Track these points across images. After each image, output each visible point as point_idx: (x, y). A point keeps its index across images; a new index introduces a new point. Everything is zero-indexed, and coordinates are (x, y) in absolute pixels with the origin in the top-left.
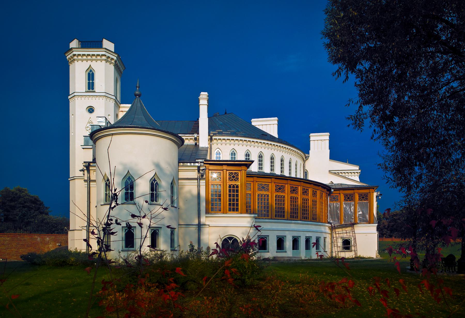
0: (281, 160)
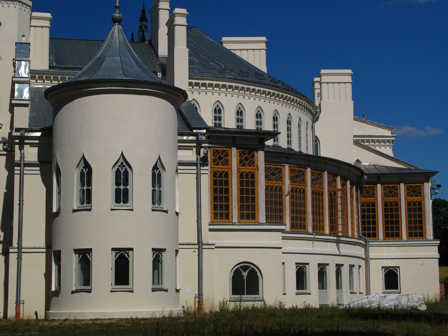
0: (274, 118)
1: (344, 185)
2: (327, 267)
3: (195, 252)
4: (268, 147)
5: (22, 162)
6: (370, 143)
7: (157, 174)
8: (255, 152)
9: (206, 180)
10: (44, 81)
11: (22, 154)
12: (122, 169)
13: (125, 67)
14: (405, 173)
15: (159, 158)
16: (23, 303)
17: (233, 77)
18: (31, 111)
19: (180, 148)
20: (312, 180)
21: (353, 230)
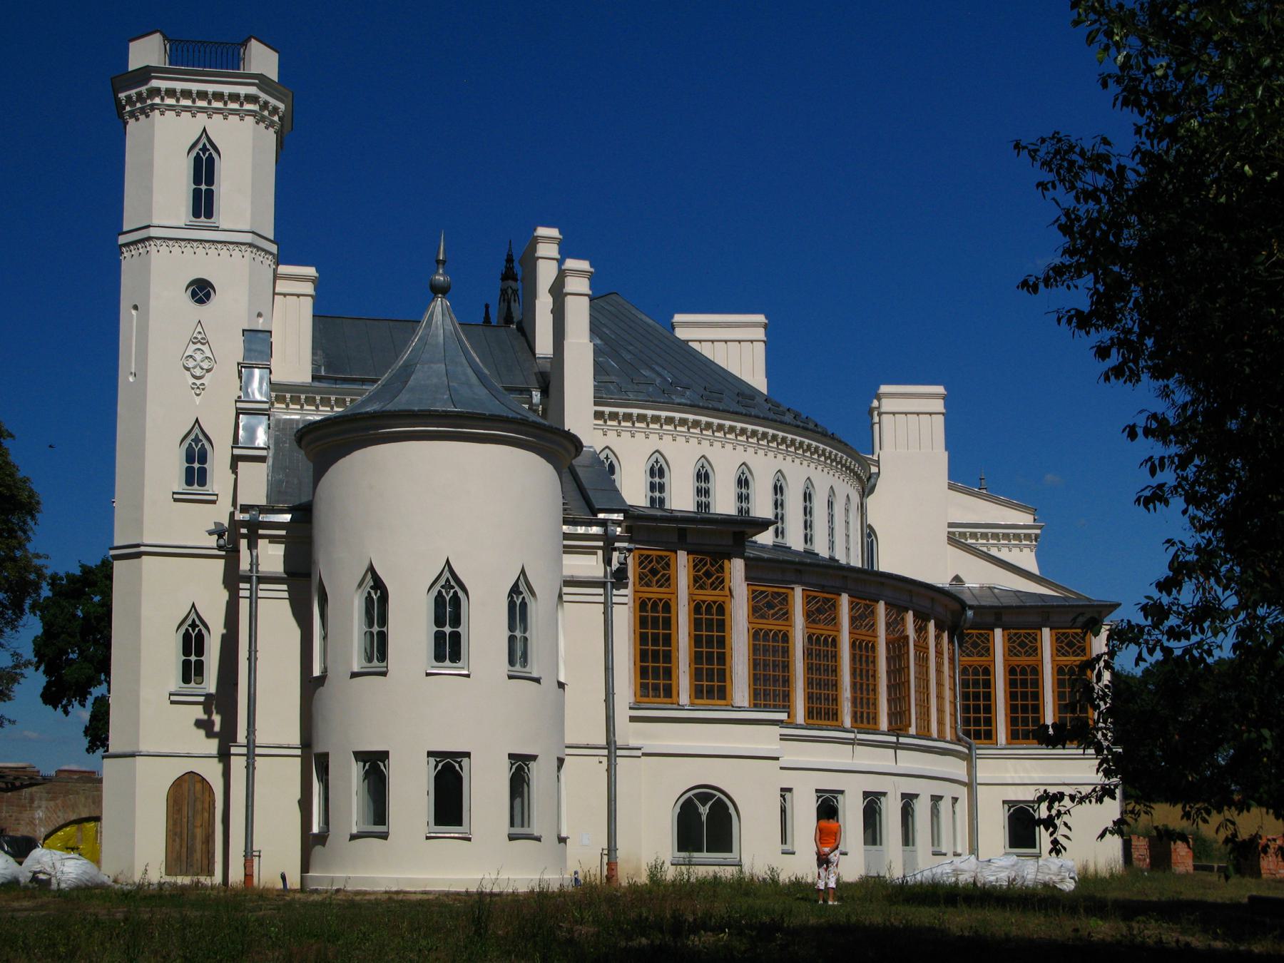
0: (775, 487)
1: (921, 630)
2: (883, 799)
3: (600, 762)
4: (763, 547)
5: (254, 574)
6: (988, 541)
7: (518, 603)
8: (726, 562)
9: (624, 617)
10: (302, 406)
11: (254, 557)
12: (447, 594)
13: (455, 384)
14: (1053, 607)
15: (523, 572)
16: (259, 856)
17: (689, 402)
18: (275, 469)
19: (568, 550)
20: (853, 620)
21: (941, 722)
